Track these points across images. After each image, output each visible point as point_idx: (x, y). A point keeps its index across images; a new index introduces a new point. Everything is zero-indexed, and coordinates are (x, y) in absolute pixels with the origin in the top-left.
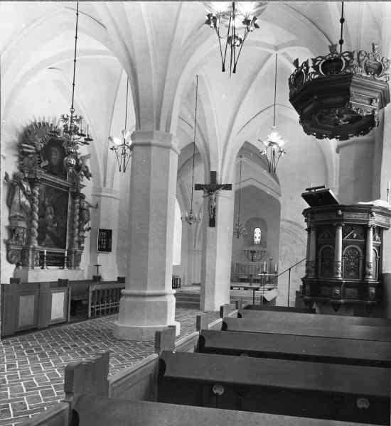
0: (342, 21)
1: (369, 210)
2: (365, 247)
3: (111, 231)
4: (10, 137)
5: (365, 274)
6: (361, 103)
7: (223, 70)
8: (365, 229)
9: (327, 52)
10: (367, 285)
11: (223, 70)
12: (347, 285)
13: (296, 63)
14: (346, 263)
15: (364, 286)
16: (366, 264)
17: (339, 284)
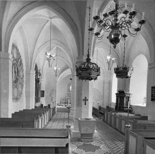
3: (44, 91)
6: (129, 75)
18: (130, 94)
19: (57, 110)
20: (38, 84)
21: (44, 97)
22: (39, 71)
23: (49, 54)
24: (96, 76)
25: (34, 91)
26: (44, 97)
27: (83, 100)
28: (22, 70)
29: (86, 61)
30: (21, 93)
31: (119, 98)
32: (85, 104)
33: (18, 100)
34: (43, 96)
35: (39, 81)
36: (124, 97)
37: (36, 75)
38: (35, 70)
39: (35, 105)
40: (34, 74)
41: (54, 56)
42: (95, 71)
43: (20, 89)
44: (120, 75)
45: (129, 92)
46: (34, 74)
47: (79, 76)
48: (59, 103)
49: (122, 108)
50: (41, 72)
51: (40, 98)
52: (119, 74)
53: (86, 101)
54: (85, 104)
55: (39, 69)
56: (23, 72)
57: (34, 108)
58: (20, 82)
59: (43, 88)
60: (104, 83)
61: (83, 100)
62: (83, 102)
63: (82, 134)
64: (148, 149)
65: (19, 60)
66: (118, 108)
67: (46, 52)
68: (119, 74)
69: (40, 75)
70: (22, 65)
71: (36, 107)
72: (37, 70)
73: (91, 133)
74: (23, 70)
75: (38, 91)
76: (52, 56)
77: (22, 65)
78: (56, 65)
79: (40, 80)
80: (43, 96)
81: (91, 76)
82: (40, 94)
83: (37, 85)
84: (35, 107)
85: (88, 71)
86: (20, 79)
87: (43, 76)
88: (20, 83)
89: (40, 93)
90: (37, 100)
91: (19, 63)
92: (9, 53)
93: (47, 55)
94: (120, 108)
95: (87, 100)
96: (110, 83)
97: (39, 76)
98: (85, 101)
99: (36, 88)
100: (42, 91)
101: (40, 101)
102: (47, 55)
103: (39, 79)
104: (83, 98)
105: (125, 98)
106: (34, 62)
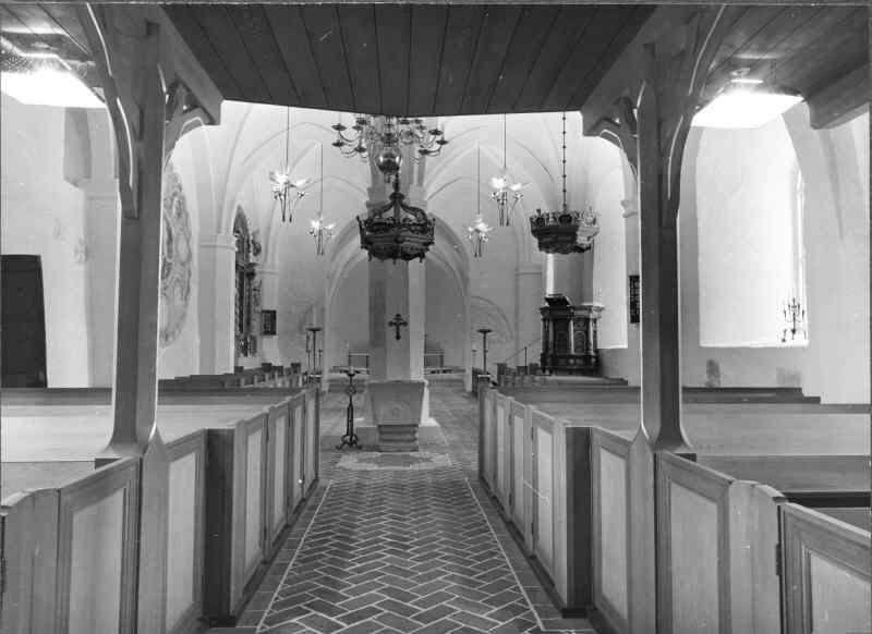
0: (564, 191)
1: (589, 309)
2: (587, 333)
3: (275, 312)
4: (527, 226)
5: (588, 349)
6: (582, 240)
7: (284, 220)
8: (587, 320)
9: (561, 210)
10: (590, 357)
11: (284, 220)
12: (579, 357)
13: (539, 211)
14: (575, 343)
15: (587, 358)
16: (588, 343)
17: (572, 357)
18: (591, 307)
19: (331, 385)
20: (250, 285)
21: (274, 333)
22: (251, 238)
23: (281, 179)
24: (419, 246)
25: (232, 310)
26: (274, 333)
27: (391, 324)
28: (185, 234)
29: (389, 201)
30: (183, 317)
31: (551, 324)
32: (398, 337)
33: (170, 339)
34: (270, 330)
35: (251, 275)
36: (568, 324)
37: (237, 249)
38: (236, 231)
39: (236, 362)
40: (232, 249)
41: (300, 183)
42: (413, 232)
43: (179, 302)
44: (551, 243)
45: (592, 301)
46: (232, 249)
47: (369, 246)
48: (342, 363)
49: (562, 361)
50: (261, 240)
51: (258, 340)
52: (545, 240)
53: (401, 327)
54: (398, 337)
55: (251, 228)
56: (188, 241)
57: (232, 371)
58: (178, 275)
59: (270, 301)
60: (517, 275)
61: (391, 324)
62: (391, 332)
63: (380, 426)
64: (831, 582)
65: (176, 199)
66: (549, 360)
67: (272, 173)
68: (545, 240)
69: (258, 251)
70: (183, 215)
71: (242, 368)
72: (247, 230)
73: (410, 422)
74: (190, 234)
75: (249, 312)
76: (292, 186)
77: (187, 215)
78: (319, 214)
79: (257, 269)
80: (270, 330)
81: (401, 245)
82: (257, 323)
83: (246, 287)
84: (239, 369)
85: (393, 232)
86: (178, 265)
87: (270, 251)
88: (178, 280)
89: (258, 320)
90: (246, 346)
91: (174, 210)
92: (230, 108)
93: (274, 180)
94: (555, 359)
95: (405, 324)
96: (541, 274)
97: (255, 255)
98: (394, 327)
99: (241, 297)
100: (268, 312)
101: (258, 350)
102: (274, 180)
103: (252, 265)
104: (390, 317)
105: (572, 322)
106: (233, 202)
